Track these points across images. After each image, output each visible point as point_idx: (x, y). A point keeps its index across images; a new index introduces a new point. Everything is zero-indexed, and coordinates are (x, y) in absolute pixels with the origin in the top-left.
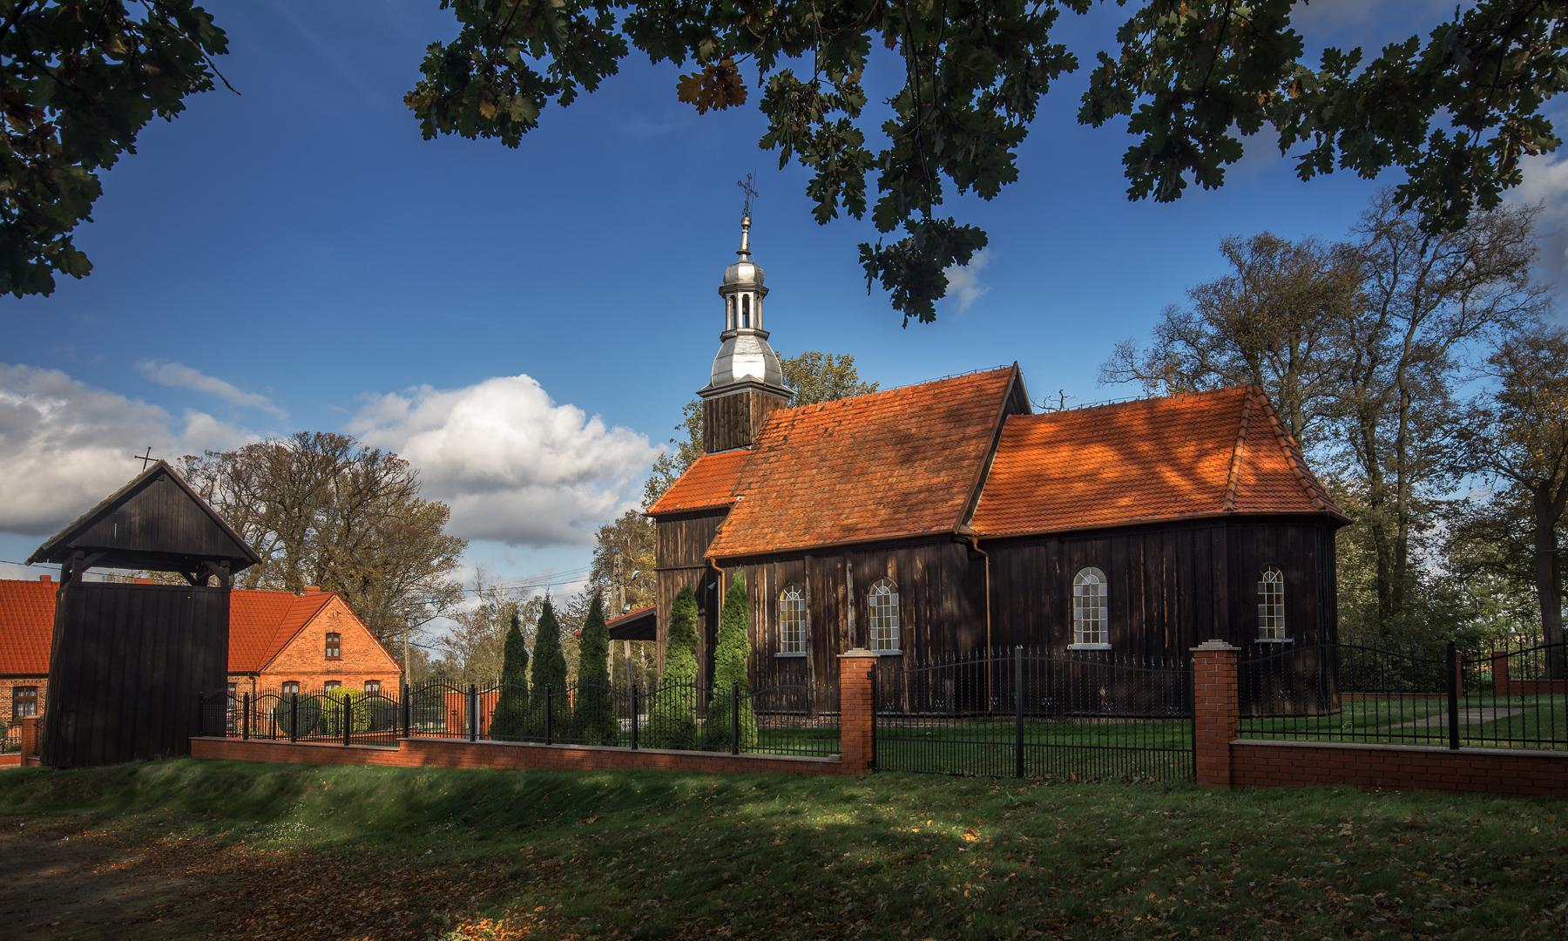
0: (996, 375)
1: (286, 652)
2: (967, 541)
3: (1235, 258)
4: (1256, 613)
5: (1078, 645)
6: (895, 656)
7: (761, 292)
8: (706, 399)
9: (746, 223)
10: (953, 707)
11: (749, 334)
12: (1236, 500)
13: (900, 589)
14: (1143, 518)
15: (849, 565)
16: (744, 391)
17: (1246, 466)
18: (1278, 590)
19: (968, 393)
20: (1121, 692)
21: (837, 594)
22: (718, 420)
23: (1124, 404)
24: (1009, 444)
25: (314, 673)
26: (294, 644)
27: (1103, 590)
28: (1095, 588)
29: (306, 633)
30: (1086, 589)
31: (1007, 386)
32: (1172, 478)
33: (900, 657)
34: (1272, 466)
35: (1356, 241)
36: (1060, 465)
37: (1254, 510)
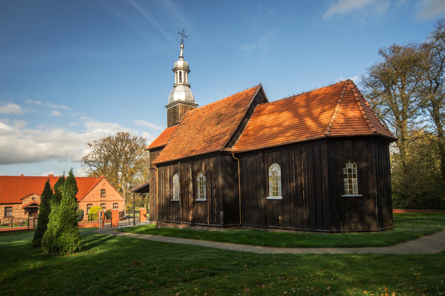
0: (255, 89)
1: (88, 195)
2: (229, 154)
3: (384, 55)
4: (343, 182)
5: (271, 197)
6: (205, 201)
7: (188, 71)
8: (168, 108)
9: (182, 46)
10: (223, 223)
11: (181, 85)
12: (331, 130)
13: (206, 175)
14: (292, 141)
15: (190, 165)
16: (177, 104)
17: (339, 115)
18: (354, 172)
19: (243, 97)
20: (286, 217)
21: (188, 177)
22: (171, 116)
23: (298, 95)
24: (256, 115)
25: (97, 201)
26: (91, 193)
27: (279, 174)
28: (277, 172)
29: (95, 189)
30: (273, 173)
31: (255, 93)
32: (309, 122)
33: (206, 202)
34: (352, 114)
35: (428, 42)
36: (271, 121)
37: (339, 134)
